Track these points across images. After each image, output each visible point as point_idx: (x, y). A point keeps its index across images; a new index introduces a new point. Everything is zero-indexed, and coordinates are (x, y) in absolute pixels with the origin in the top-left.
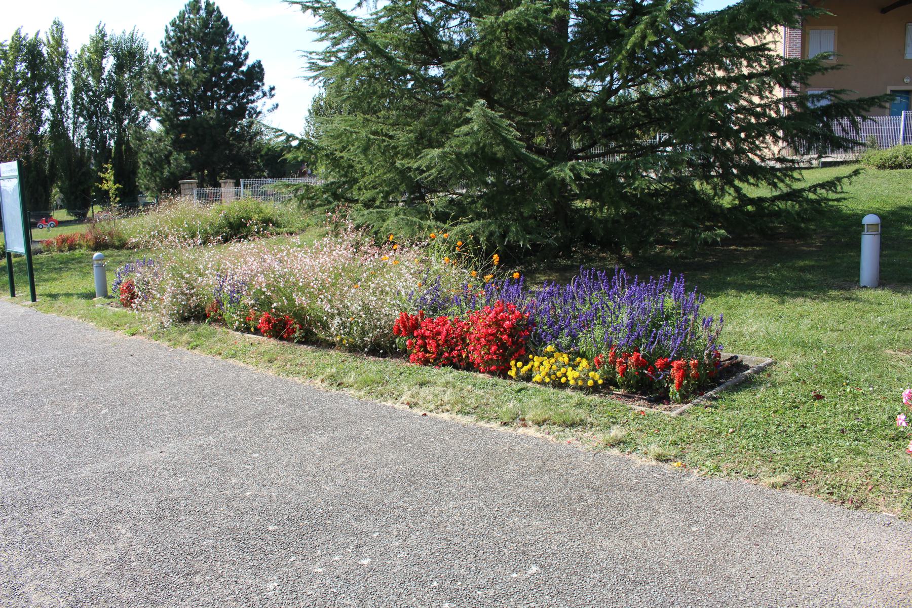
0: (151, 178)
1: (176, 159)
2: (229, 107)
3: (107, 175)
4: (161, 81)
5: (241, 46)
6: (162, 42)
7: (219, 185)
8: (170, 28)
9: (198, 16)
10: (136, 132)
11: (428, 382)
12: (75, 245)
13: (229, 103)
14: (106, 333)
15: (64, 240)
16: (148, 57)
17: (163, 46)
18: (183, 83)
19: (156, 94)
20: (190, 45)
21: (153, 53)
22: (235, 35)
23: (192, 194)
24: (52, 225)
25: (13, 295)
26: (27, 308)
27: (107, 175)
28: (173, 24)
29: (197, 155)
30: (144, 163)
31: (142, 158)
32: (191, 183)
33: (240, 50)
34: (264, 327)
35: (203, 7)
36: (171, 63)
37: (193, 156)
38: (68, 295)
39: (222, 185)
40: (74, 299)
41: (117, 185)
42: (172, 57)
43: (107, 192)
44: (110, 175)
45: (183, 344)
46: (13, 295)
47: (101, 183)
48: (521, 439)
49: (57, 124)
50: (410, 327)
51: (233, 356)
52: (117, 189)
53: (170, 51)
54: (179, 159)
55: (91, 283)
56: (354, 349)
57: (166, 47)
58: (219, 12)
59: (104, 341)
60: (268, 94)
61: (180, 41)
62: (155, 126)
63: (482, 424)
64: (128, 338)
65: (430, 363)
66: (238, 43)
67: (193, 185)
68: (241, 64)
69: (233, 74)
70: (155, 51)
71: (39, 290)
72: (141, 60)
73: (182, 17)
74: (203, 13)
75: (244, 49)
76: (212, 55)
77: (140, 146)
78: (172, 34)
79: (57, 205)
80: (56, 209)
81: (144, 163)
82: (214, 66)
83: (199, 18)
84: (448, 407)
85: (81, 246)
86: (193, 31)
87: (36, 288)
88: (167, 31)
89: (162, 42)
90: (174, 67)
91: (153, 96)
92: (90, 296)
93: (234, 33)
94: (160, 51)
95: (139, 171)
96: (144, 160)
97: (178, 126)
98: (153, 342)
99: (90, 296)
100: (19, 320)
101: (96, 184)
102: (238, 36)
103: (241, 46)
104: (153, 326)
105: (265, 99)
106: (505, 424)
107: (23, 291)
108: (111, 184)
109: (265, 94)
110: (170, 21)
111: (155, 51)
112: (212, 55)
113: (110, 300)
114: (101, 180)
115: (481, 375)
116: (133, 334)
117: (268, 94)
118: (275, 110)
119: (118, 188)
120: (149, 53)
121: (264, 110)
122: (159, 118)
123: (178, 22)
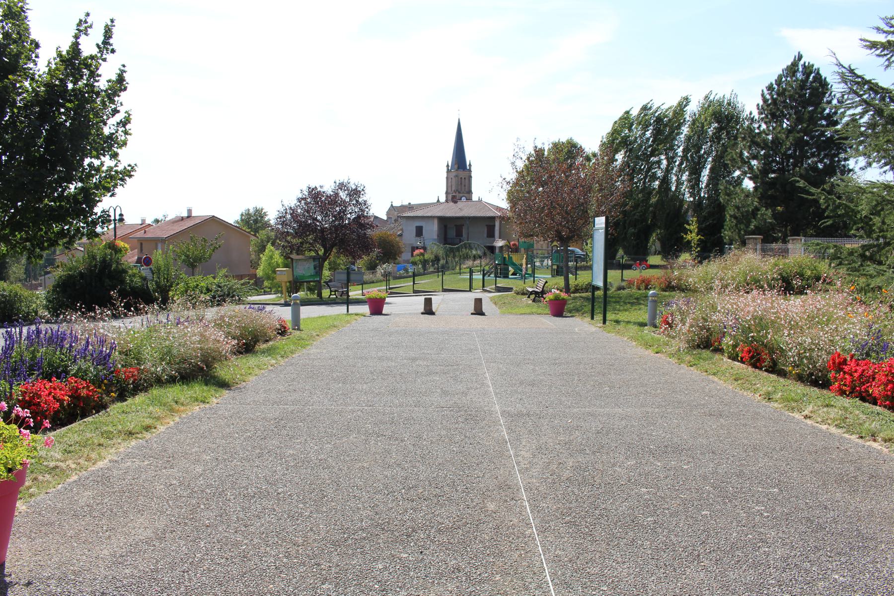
0: (735, 231)
1: (762, 215)
2: (820, 166)
3: (692, 227)
4: (754, 139)
6: (758, 105)
9: (794, 78)
10: (726, 188)
13: (821, 161)
16: (743, 120)
17: (758, 109)
18: (776, 142)
19: (748, 153)
21: (749, 116)
24: (644, 268)
25: (592, 318)
27: (692, 227)
28: (770, 88)
29: (783, 212)
30: (731, 216)
31: (730, 211)
32: (756, 239)
34: (747, 357)
35: (801, 69)
37: (780, 213)
38: (628, 322)
40: (630, 326)
43: (689, 242)
45: (686, 362)
46: (592, 318)
47: (686, 234)
48: (870, 450)
49: (665, 181)
50: (840, 365)
51: (714, 374)
54: (766, 214)
56: (800, 378)
57: (761, 111)
58: (818, 73)
59: (635, 354)
62: (748, 184)
63: (846, 435)
65: (846, 394)
67: (758, 240)
68: (836, 123)
69: (826, 133)
70: (751, 113)
72: (737, 122)
73: (779, 82)
74: (799, 76)
77: (728, 200)
78: (768, 97)
80: (655, 254)
81: (731, 216)
82: (808, 126)
83: (794, 81)
84: (829, 421)
89: (758, 105)
91: (746, 154)
92: (642, 325)
94: (756, 114)
95: (726, 223)
96: (732, 213)
97: (767, 183)
98: (668, 359)
99: (642, 325)
104: (674, 349)
107: (599, 317)
108: (694, 234)
110: (767, 85)
111: (751, 113)
112: (806, 116)
113: (654, 329)
115: (878, 408)
116: (657, 353)
119: (700, 239)
120: (745, 116)
121: (857, 169)
122: (749, 175)
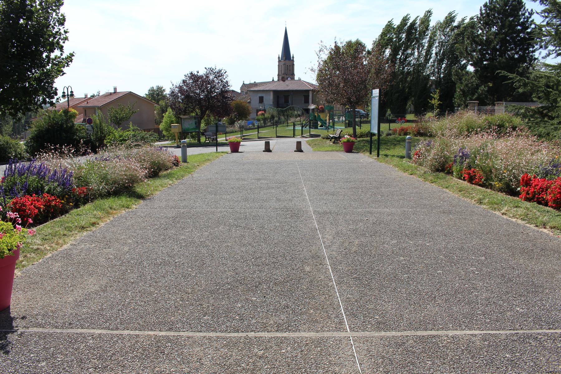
3: (435, 96)
5: (529, 16)
7: (494, 105)
8: (483, 8)
11: (520, 207)
12: (408, 133)
14: (401, 173)
15: (402, 129)
20: (495, 17)
22: (526, 9)
23: (474, 110)
24: (403, 122)
25: (371, 153)
26: (374, 160)
27: (435, 96)
28: (485, 6)
32: (474, 103)
33: (528, 18)
36: (481, 29)
38: (393, 156)
39: (496, 105)
40: (395, 158)
41: (439, 102)
42: (483, 26)
43: (433, 105)
44: (436, 96)
48: (542, 233)
51: (447, 188)
52: (439, 104)
53: (482, 22)
55: (403, 152)
60: (543, 47)
61: (488, 15)
62: (471, 69)
63: (528, 225)
64: (408, 176)
66: (527, 14)
67: (475, 104)
68: (528, 28)
71: (381, 152)
75: (530, 17)
76: (507, 23)
79: (411, 112)
80: (410, 113)
84: (517, 216)
85: (410, 133)
86: (496, 9)
87: (380, 151)
88: (481, 10)
90: (483, 32)
92: (402, 157)
93: (525, 8)
95: (455, 94)
99: (402, 157)
100: (368, 164)
101: (428, 100)
102: (527, 10)
103: (529, 16)
105: (541, 50)
106: (537, 226)
107: (375, 153)
109: (541, 47)
114: (431, 98)
116: (411, 175)
117: (543, 47)
118: (547, 58)
123: (488, 4)
